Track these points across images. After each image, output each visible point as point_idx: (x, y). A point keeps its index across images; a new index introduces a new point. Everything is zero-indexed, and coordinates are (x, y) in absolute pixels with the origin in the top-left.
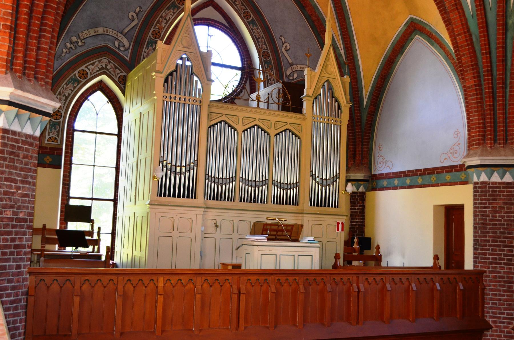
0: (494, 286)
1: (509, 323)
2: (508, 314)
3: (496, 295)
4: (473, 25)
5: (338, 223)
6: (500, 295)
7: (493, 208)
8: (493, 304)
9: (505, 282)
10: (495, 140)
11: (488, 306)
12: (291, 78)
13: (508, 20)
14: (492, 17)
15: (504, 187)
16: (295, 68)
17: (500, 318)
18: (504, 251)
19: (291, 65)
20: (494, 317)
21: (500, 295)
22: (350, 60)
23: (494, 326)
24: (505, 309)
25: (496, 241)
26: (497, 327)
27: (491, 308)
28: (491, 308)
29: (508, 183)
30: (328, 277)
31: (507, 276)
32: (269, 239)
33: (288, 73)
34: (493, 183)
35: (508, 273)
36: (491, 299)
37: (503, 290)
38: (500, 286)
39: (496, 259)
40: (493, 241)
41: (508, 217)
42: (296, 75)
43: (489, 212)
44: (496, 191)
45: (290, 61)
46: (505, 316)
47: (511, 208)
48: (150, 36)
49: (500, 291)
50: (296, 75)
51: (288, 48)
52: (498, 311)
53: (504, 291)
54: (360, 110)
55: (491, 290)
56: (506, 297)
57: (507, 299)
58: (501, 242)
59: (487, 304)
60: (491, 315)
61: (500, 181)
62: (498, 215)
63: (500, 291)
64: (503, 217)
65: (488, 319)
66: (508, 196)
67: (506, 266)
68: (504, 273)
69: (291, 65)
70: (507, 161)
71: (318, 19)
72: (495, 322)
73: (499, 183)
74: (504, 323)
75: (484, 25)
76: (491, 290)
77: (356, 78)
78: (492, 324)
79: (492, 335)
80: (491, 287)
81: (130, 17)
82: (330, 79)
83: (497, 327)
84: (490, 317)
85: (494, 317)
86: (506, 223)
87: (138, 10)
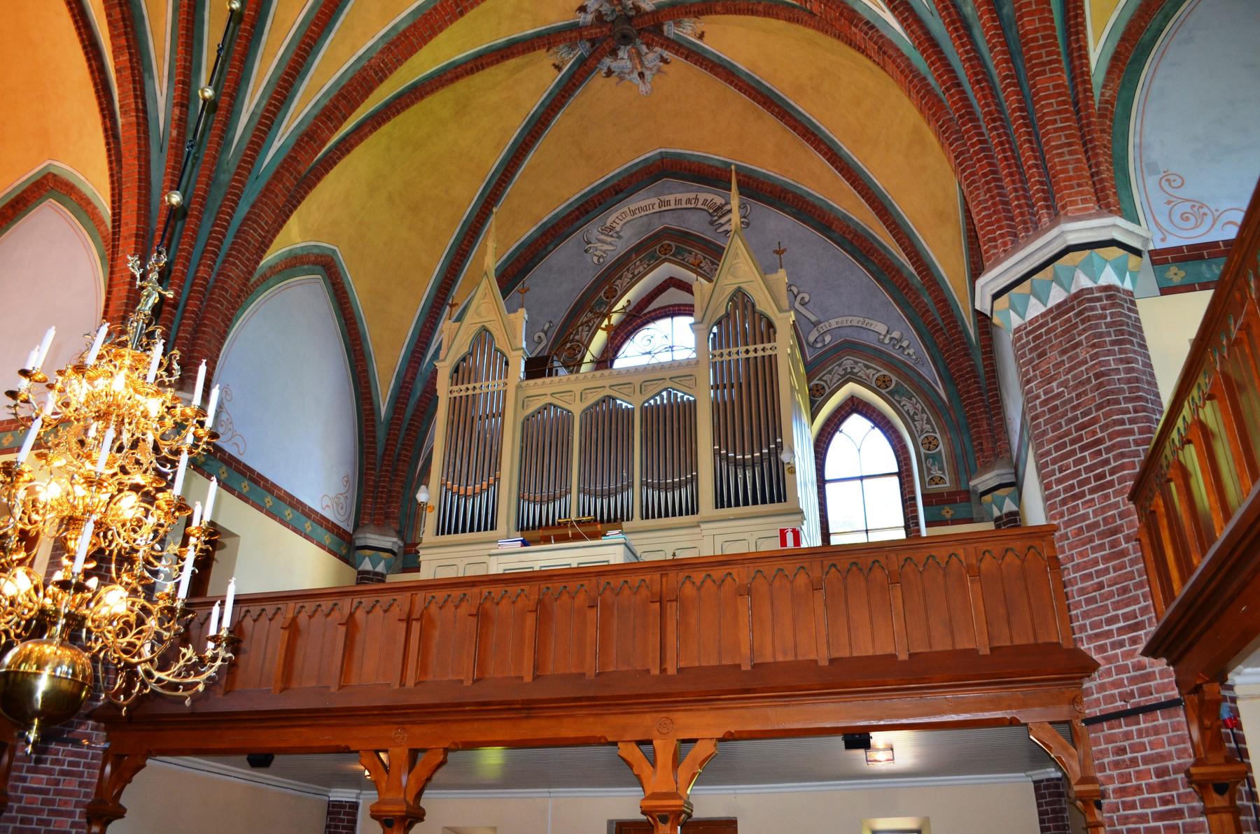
0: (1081, 554)
1: (1134, 641)
2: (1126, 617)
3: (1089, 576)
4: (919, 61)
5: (783, 533)
6: (1099, 574)
7: (1043, 374)
8: (1088, 602)
9: (1102, 535)
10: (280, 86)
11: (1078, 611)
12: (819, 345)
13: (964, 10)
14: (937, 26)
15: (1053, 319)
16: (824, 327)
17: (1108, 634)
18: (1083, 460)
19: (815, 324)
20: (1098, 636)
21: (1099, 574)
22: (266, 125)
23: (1101, 661)
24: (1117, 606)
25: (1064, 445)
26: (1108, 660)
27: (1086, 615)
28: (1086, 615)
29: (1059, 306)
30: (594, 580)
31: (1104, 519)
32: (524, 543)
33: (811, 339)
34: (1031, 322)
35: (1103, 510)
36: (1082, 591)
37: (1103, 557)
38: (1094, 550)
39: (1072, 487)
40: (1057, 449)
41: (1074, 378)
42: (828, 339)
43: (1038, 387)
44: (1041, 336)
45: (813, 318)
46: (1122, 624)
47: (1077, 355)
48: (1204, 553)
49: (1096, 562)
50: (828, 339)
51: (807, 299)
52: (1103, 617)
53: (1106, 559)
54: (967, 355)
55: (1077, 568)
56: (1112, 574)
57: (1115, 578)
58: (1073, 442)
59: (1076, 608)
60: (1090, 632)
61: (1043, 310)
62: (1054, 384)
63: (1096, 562)
64: (1064, 384)
65: (1084, 647)
66: (1064, 332)
67: (1095, 496)
68: (1095, 513)
69: (815, 324)
70: (1036, 257)
71: (856, 234)
72: (1101, 649)
73: (1043, 315)
74: (1121, 644)
75: (928, 43)
76: (1077, 568)
77: (945, 300)
78: (1096, 657)
79: (1102, 688)
80: (1076, 561)
81: (536, 338)
82: (742, 285)
83: (1108, 660)
84: (1090, 638)
85: (1098, 636)
86: (1074, 394)
87: (547, 326)
